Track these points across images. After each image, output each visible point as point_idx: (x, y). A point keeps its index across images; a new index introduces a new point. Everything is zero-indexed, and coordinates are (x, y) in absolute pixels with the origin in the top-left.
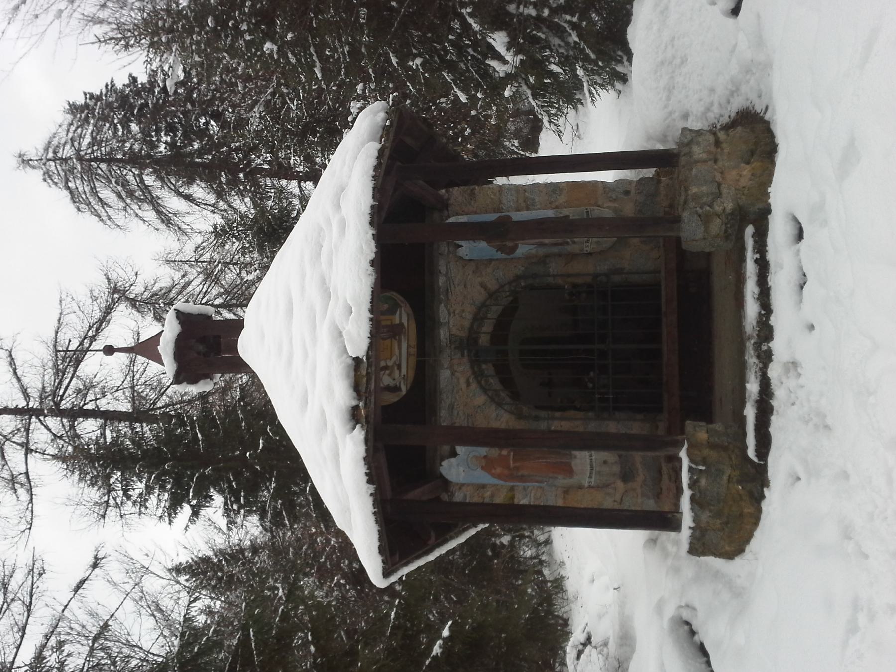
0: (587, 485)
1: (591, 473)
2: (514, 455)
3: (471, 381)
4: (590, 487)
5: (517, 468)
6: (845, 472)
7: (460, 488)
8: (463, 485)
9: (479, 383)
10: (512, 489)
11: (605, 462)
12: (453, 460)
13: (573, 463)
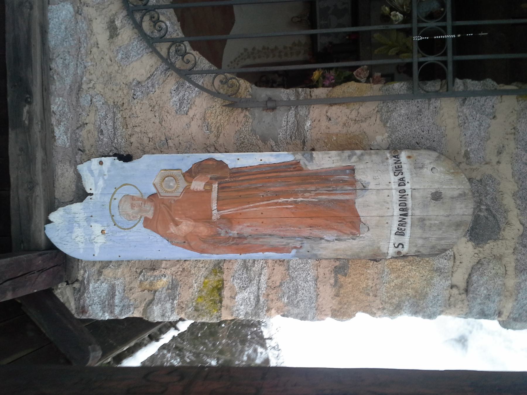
0: (392, 251)
1: (402, 223)
2: (221, 189)
3: (118, 23)
4: (399, 256)
5: (228, 220)
6: (154, 269)
7: (100, 273)
8: (106, 264)
9: (138, 26)
10: (218, 268)
11: (437, 196)
12: (76, 207)
13: (359, 202)
